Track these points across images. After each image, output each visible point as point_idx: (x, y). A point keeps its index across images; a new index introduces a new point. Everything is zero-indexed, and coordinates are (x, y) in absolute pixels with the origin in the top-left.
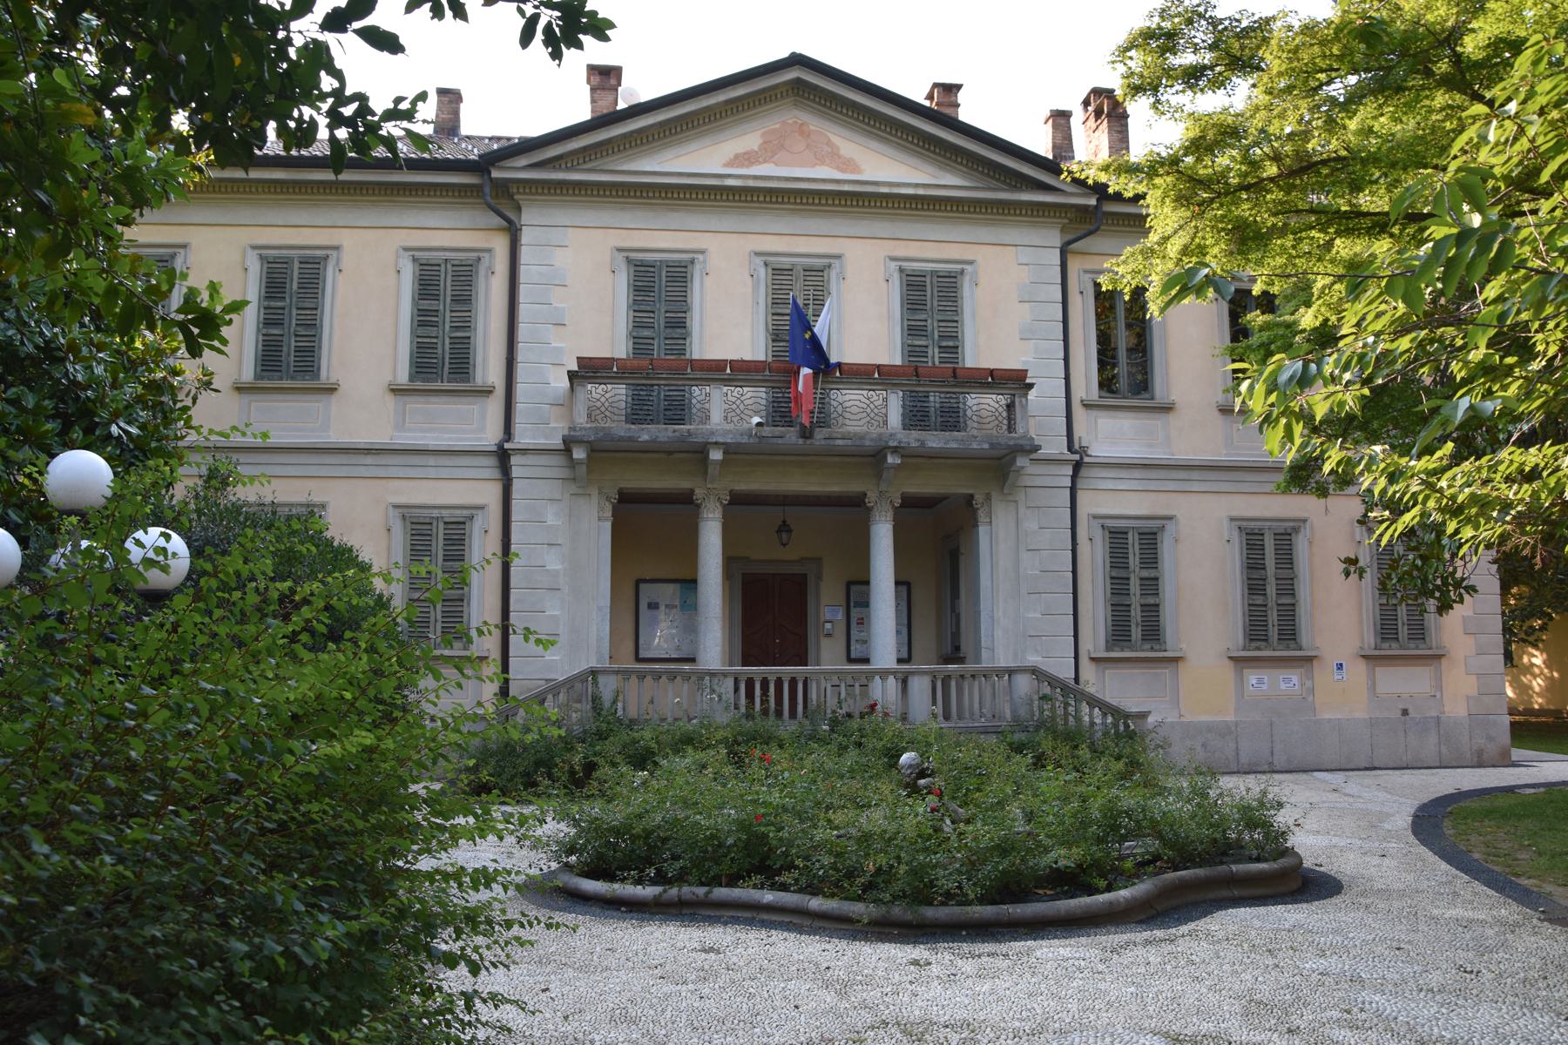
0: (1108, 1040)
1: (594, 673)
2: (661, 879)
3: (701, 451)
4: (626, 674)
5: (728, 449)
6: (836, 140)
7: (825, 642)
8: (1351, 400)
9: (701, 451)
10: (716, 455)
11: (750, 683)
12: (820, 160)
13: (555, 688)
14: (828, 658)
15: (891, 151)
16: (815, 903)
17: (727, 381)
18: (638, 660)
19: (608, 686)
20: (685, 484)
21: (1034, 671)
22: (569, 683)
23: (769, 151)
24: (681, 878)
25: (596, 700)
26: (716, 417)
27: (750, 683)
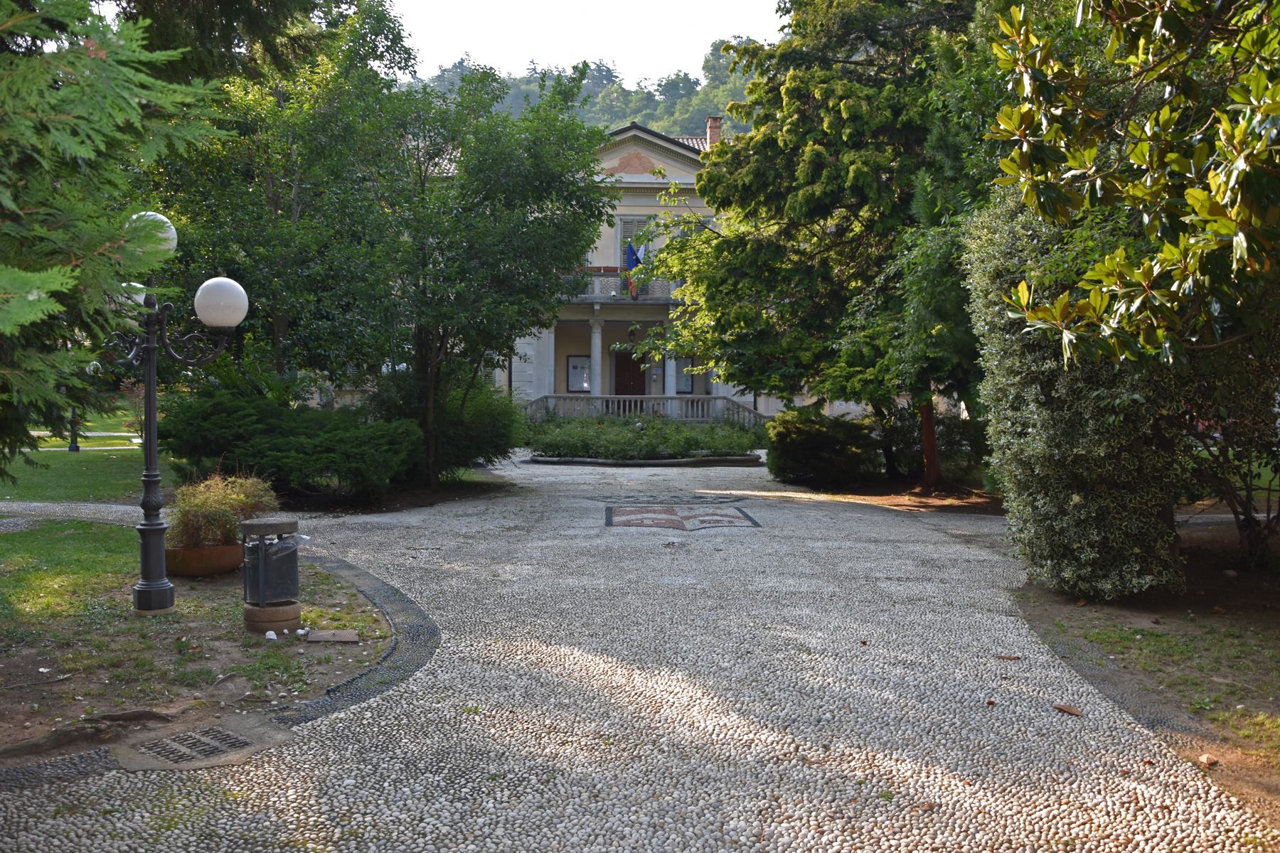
0: (1260, 848)
1: (546, 397)
2: (559, 455)
3: (592, 305)
4: (559, 398)
5: (602, 304)
6: (653, 161)
7: (653, 384)
8: (162, 510)
9: (592, 305)
10: (597, 307)
11: (607, 402)
12: (645, 171)
13: (532, 404)
14: (653, 393)
15: (679, 165)
16: (600, 461)
17: (602, 276)
18: (569, 391)
19: (551, 403)
20: (585, 318)
21: (724, 398)
22: (537, 401)
23: (624, 167)
24: (565, 455)
25: (547, 409)
26: (597, 291)
27: (607, 402)
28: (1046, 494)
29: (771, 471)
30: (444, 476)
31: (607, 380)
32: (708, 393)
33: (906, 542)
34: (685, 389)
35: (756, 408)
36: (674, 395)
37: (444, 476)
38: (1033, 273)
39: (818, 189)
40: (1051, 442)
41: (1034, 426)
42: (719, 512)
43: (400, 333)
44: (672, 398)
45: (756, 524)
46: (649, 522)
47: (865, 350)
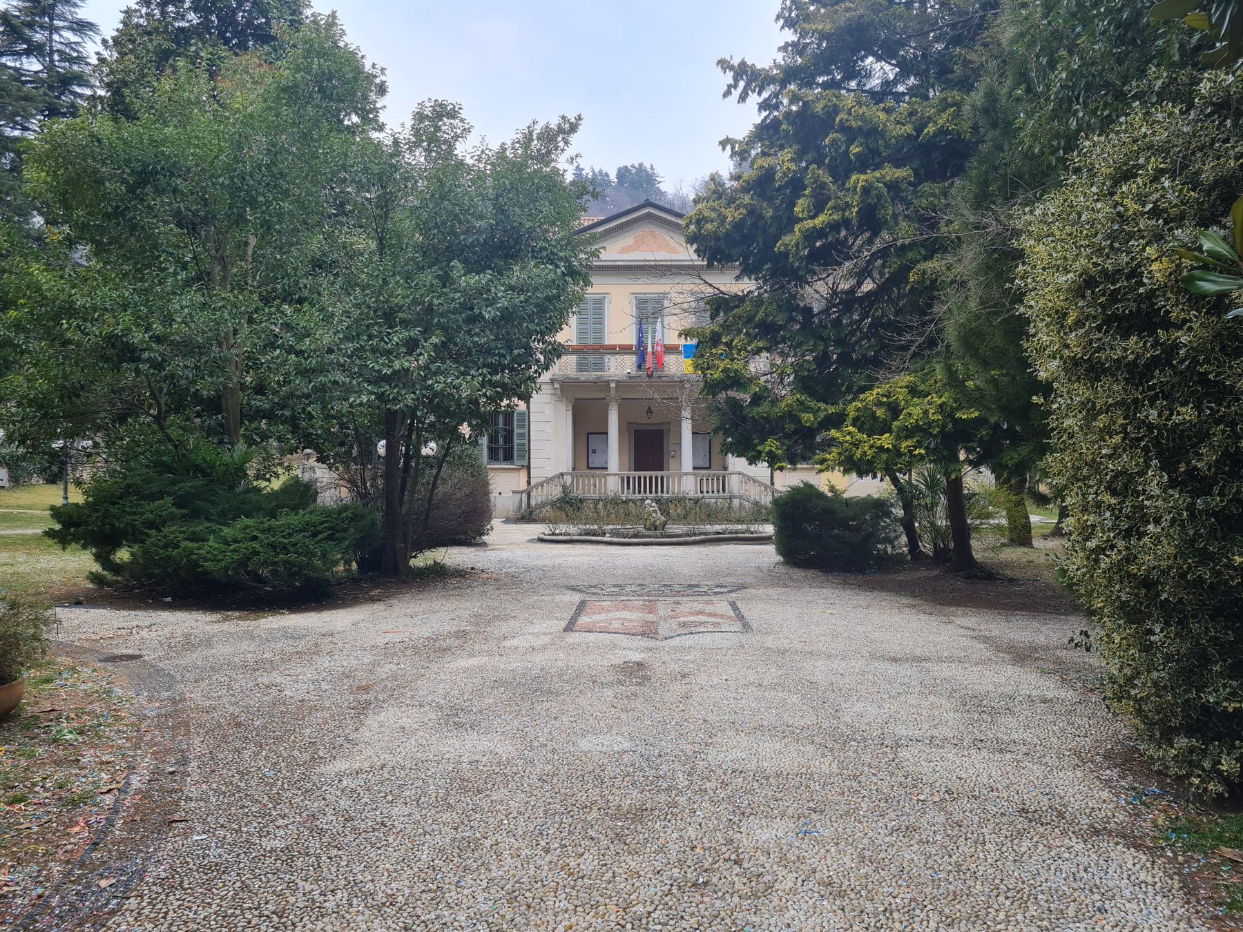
5: (618, 382)
10: (613, 385)
18: (589, 468)
21: (740, 473)
28: (1167, 624)
29: (781, 551)
30: (421, 560)
31: (627, 457)
32: (725, 468)
33: (940, 660)
34: (702, 464)
35: (772, 484)
36: (691, 470)
37: (421, 560)
38: (1154, 267)
39: (820, 220)
40: (1189, 547)
41: (1157, 521)
42: (709, 608)
43: (276, 392)
44: (686, 474)
45: (746, 627)
46: (616, 625)
47: (880, 412)
